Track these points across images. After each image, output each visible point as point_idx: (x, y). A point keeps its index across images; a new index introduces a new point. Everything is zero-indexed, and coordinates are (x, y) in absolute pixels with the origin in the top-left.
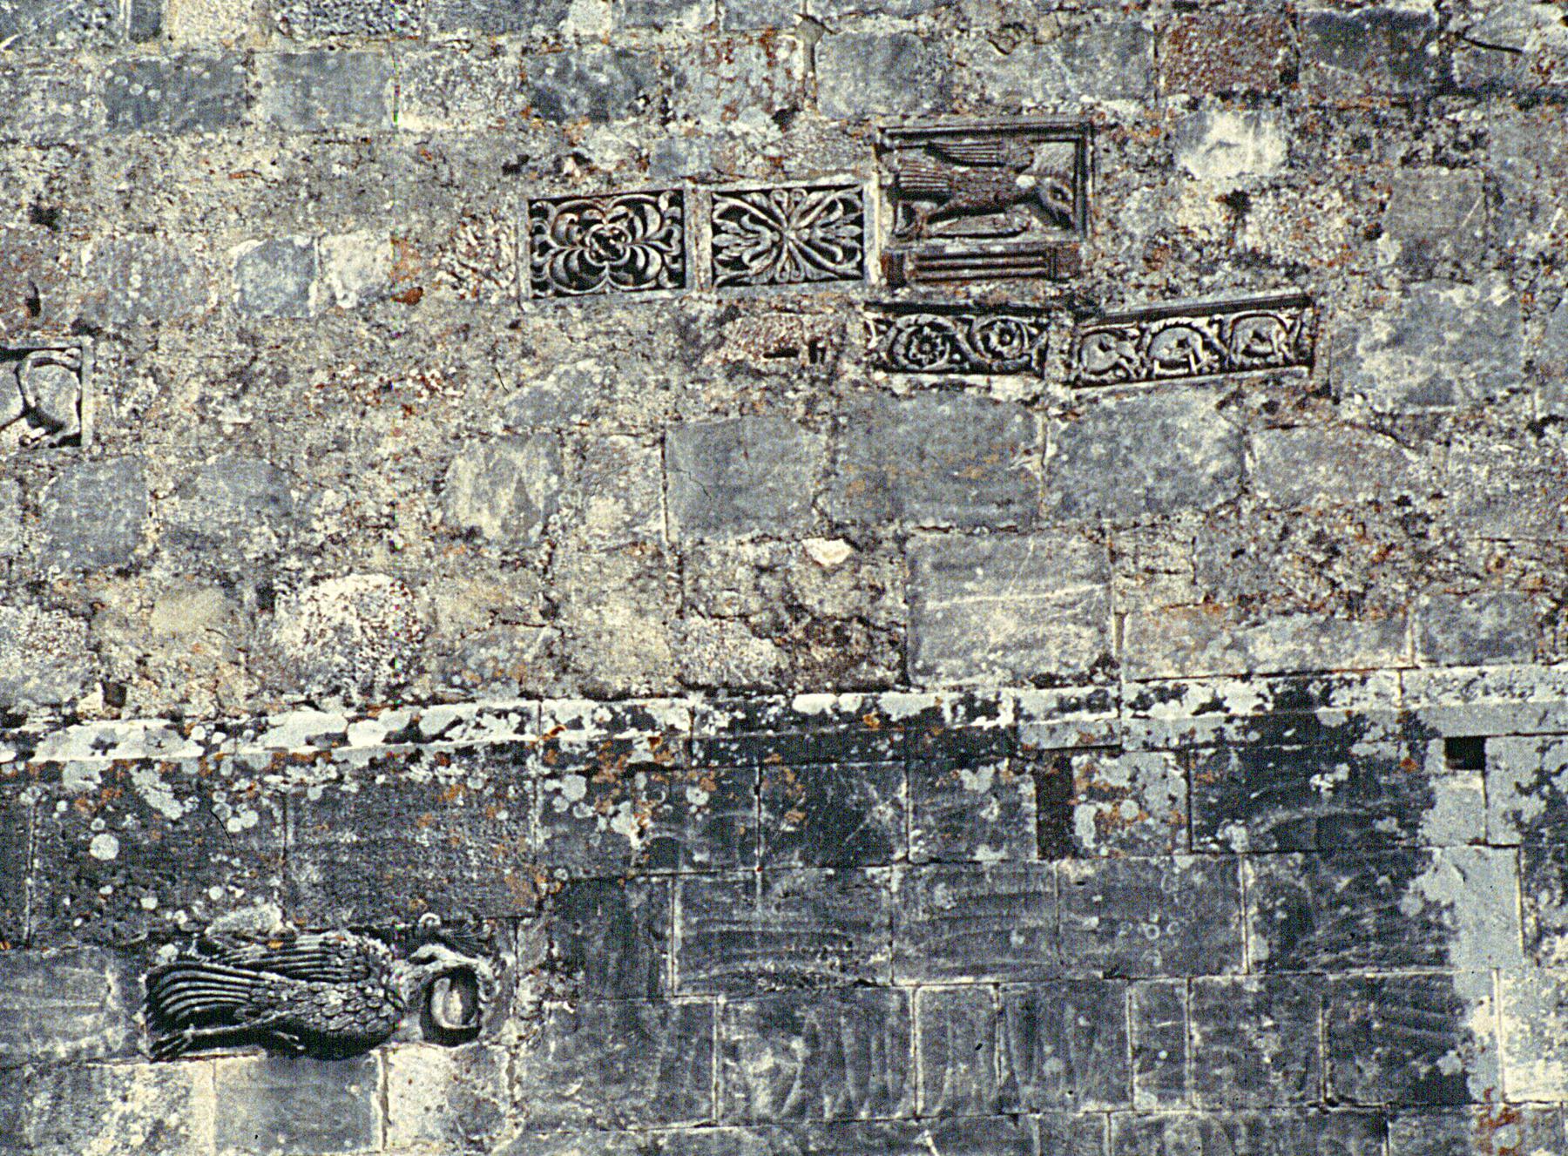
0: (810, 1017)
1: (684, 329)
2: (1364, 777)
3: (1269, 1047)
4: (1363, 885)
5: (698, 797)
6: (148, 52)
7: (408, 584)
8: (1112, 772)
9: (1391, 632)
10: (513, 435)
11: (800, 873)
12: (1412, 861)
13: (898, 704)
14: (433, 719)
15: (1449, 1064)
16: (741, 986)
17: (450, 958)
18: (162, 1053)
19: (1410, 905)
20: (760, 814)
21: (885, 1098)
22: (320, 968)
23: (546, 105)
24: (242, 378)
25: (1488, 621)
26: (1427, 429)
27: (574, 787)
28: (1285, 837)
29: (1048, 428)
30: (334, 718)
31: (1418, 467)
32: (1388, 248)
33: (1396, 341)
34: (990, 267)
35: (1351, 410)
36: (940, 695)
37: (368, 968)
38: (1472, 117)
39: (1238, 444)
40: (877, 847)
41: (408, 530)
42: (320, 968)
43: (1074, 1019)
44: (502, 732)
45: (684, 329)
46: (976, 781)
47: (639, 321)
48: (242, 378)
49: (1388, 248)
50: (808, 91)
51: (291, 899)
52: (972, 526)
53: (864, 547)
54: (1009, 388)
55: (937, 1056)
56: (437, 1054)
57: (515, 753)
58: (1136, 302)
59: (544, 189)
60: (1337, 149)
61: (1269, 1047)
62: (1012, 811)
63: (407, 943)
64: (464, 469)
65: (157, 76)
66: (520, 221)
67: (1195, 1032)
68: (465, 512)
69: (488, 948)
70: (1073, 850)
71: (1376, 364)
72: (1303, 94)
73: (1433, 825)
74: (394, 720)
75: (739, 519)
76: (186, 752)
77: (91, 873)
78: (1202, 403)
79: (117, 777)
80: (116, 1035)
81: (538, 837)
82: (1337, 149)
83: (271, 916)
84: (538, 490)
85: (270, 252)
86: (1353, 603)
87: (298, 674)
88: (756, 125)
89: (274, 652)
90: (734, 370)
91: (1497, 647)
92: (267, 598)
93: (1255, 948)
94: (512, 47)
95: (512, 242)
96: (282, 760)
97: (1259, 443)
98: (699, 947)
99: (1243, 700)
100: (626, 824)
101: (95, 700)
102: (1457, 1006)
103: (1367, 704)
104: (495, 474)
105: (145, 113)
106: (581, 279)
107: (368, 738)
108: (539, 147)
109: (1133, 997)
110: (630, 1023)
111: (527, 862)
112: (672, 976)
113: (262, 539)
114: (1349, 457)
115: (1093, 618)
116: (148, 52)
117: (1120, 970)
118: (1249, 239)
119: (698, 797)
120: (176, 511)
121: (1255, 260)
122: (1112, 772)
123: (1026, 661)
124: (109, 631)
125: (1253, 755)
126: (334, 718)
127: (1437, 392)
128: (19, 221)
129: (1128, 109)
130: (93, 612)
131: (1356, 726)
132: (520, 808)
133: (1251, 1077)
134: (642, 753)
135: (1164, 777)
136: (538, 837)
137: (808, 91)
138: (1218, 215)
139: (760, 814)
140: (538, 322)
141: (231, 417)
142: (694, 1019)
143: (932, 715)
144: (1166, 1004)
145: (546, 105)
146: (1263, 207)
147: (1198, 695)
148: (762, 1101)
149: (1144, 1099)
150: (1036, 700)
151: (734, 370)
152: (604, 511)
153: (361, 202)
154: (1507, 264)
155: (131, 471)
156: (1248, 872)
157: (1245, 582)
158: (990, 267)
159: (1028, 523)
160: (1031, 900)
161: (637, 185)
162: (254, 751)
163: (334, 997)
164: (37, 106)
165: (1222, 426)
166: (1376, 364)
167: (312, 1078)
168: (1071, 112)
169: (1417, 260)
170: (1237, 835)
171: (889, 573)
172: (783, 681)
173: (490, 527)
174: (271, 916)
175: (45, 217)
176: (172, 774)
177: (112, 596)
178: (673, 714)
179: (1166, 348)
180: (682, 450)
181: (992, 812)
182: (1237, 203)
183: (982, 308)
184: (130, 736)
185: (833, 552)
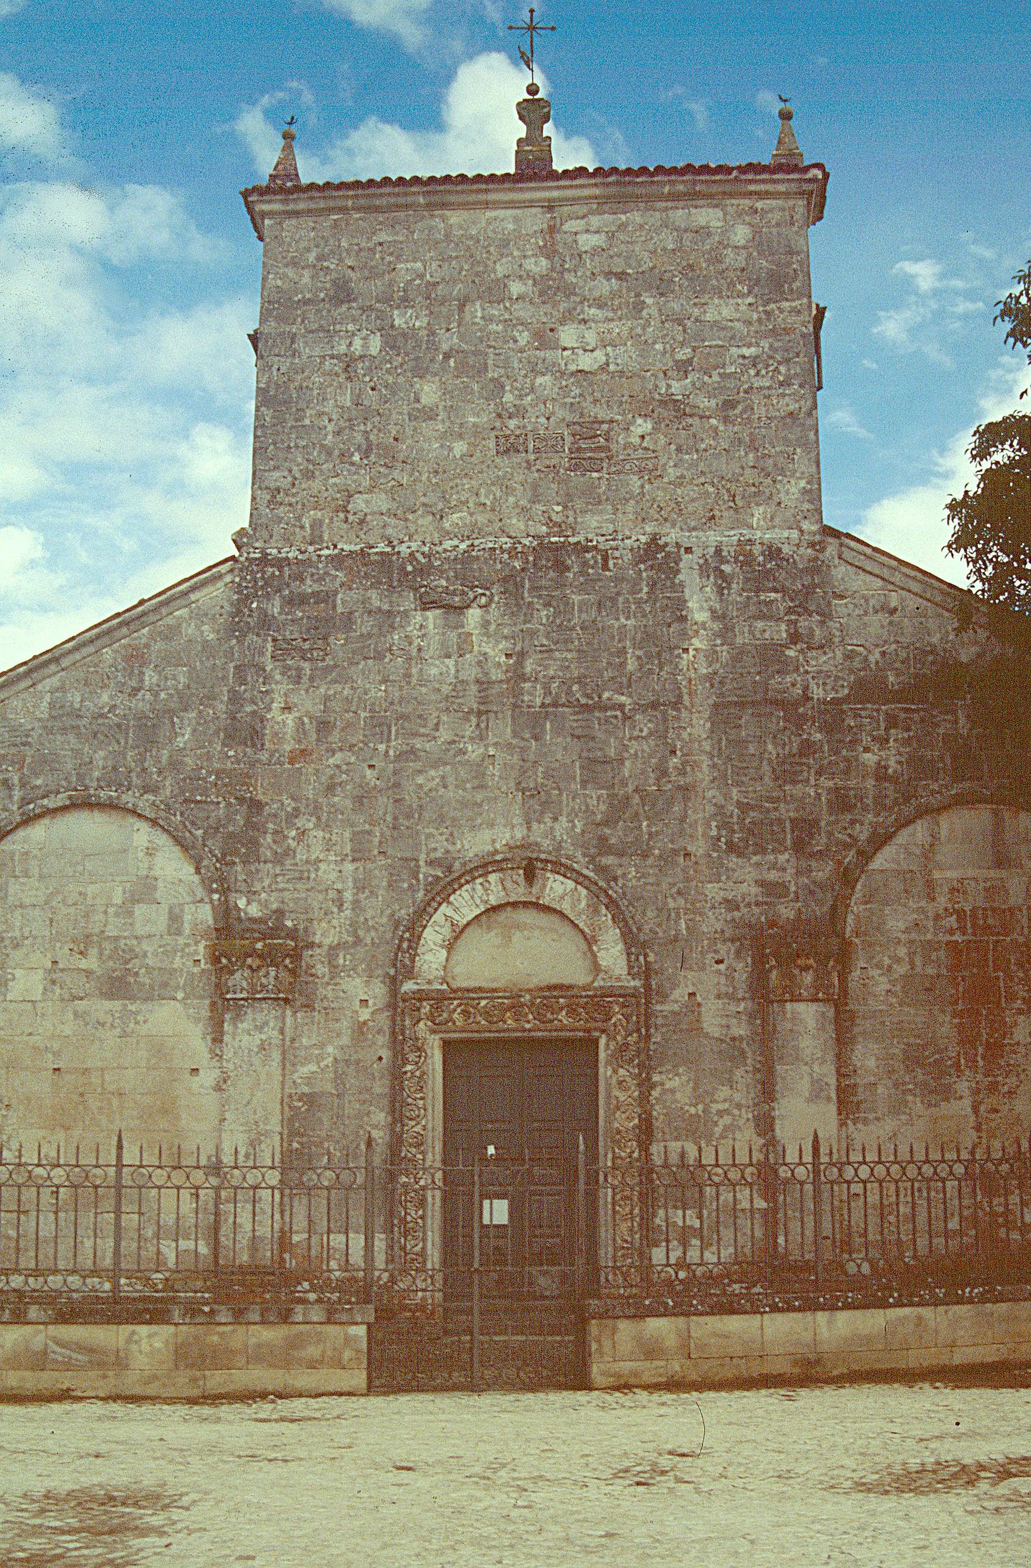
0: (554, 604)
1: (528, 462)
2: (668, 555)
3: (648, 609)
4: (668, 578)
5: (531, 558)
6: (417, 405)
7: (471, 514)
8: (617, 554)
9: (673, 526)
10: (493, 484)
11: (552, 574)
12: (678, 572)
13: (571, 540)
14: (476, 542)
15: (684, 613)
16: (540, 597)
17: (480, 591)
18: (424, 609)
19: (677, 581)
20: (544, 562)
21: (569, 621)
22: (454, 593)
23: (499, 416)
24: (436, 472)
25: (693, 524)
26: (681, 484)
27: (506, 556)
28: (652, 567)
29: (604, 483)
30: (456, 542)
31: (679, 492)
32: (673, 447)
33: (675, 466)
34: (592, 450)
35: (666, 480)
36: (580, 538)
37: (463, 593)
38: (690, 420)
39: (642, 487)
40: (568, 569)
41: (471, 505)
42: (454, 593)
43: (609, 604)
44: (491, 545)
45: (528, 462)
46: (588, 556)
47: (519, 460)
48: (436, 472)
49: (673, 447)
50: (553, 413)
51: (448, 579)
52: (588, 503)
53: (565, 507)
54: (595, 475)
55: (580, 611)
56: (478, 610)
57: (494, 549)
58: (621, 457)
59: (498, 433)
60: (663, 426)
61: (648, 609)
62: (596, 562)
63: (472, 588)
64: (483, 491)
65: (419, 410)
66: (493, 439)
67: (633, 607)
68: (483, 500)
69: (487, 589)
70: (609, 570)
71: (670, 470)
72: (655, 415)
73: (682, 565)
74: (469, 543)
75: (539, 502)
76: (426, 549)
77: (407, 574)
78: (635, 478)
79: (412, 554)
80: (413, 606)
81: (499, 566)
82: (663, 426)
83: (444, 583)
84: (498, 494)
85: (442, 446)
86: (666, 520)
87: (448, 533)
88: (542, 420)
89: (443, 528)
90: (538, 471)
91: (694, 529)
92: (442, 517)
93: (646, 589)
94: (492, 403)
95: (492, 444)
96: (445, 551)
97: (647, 486)
98: (533, 588)
99: (643, 539)
100: (516, 564)
101: (406, 539)
102: (686, 601)
103: (668, 540)
104: (490, 492)
105: (416, 418)
106: (507, 451)
107: (463, 546)
108: (498, 424)
109: (621, 599)
110: (517, 605)
111: (496, 571)
112: (526, 595)
113: (440, 506)
114: (665, 490)
115: (613, 522)
116: (417, 405)
117: (618, 594)
118: (645, 444)
119: (531, 558)
120: (423, 499)
121: (646, 449)
122: (617, 554)
123: (598, 531)
124: (409, 524)
125: (645, 550)
126: (456, 542)
127: (682, 477)
128: (391, 440)
129: (619, 418)
130: (406, 520)
131: (666, 544)
132: (495, 560)
133: (644, 616)
134: (519, 549)
135: (752, 1542)
136: (499, 566)
137: (553, 413)
138: (638, 440)
139: (544, 562)
140: (498, 460)
141: (434, 481)
142: (530, 603)
143: (579, 542)
144: (627, 601)
145: (499, 416)
146: (647, 438)
147: (634, 538)
148: (544, 621)
149: (623, 620)
150: (601, 539)
151: (538, 471)
152: (511, 499)
153: (461, 436)
154: (697, 451)
155: (414, 492)
156: (644, 574)
157: (643, 515)
158: (592, 450)
159: (599, 503)
160: (600, 580)
161: (518, 432)
162: (439, 549)
163: (457, 599)
164: (394, 416)
165: (639, 483)
166: (670, 470)
167: (453, 618)
168: (608, 418)
169: (679, 450)
170: (642, 566)
171: (571, 513)
172: (548, 535)
173: (488, 503)
174: (444, 583)
175: (396, 439)
176: (423, 554)
177: (410, 517)
178: (526, 541)
179: (627, 467)
180: (527, 487)
181: (592, 562)
182: (643, 437)
183: (590, 458)
184: (414, 546)
185: (559, 508)
